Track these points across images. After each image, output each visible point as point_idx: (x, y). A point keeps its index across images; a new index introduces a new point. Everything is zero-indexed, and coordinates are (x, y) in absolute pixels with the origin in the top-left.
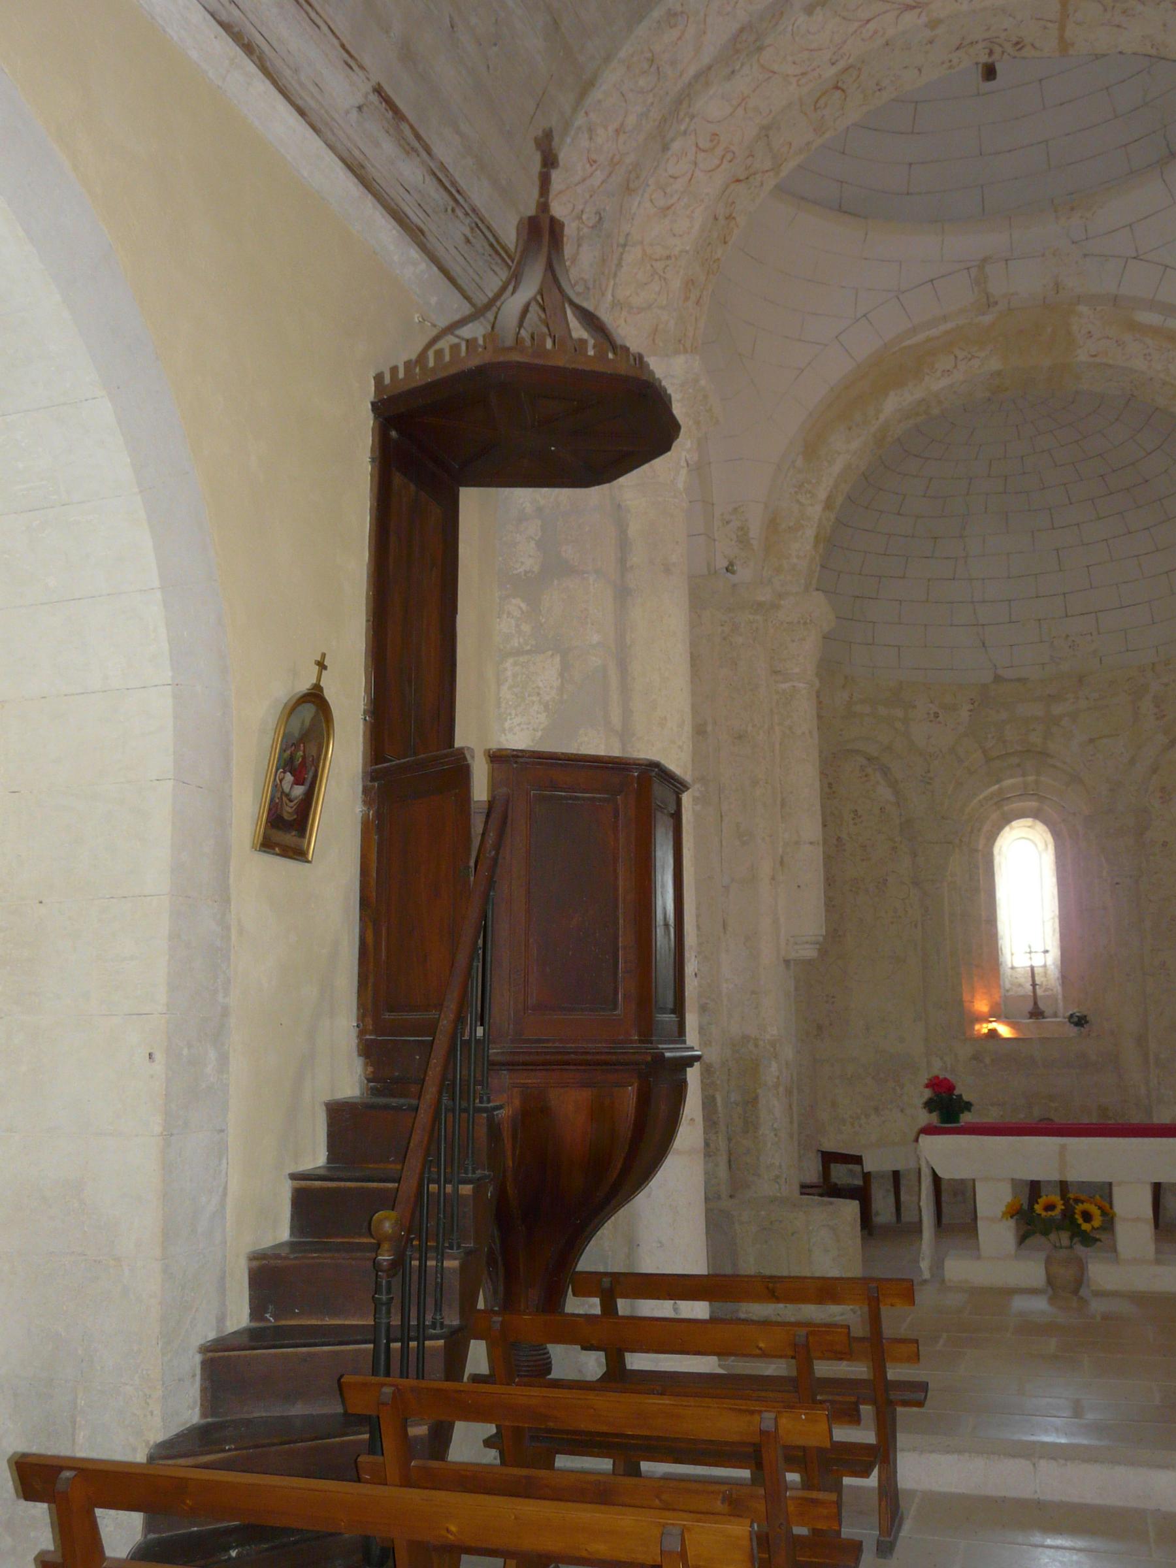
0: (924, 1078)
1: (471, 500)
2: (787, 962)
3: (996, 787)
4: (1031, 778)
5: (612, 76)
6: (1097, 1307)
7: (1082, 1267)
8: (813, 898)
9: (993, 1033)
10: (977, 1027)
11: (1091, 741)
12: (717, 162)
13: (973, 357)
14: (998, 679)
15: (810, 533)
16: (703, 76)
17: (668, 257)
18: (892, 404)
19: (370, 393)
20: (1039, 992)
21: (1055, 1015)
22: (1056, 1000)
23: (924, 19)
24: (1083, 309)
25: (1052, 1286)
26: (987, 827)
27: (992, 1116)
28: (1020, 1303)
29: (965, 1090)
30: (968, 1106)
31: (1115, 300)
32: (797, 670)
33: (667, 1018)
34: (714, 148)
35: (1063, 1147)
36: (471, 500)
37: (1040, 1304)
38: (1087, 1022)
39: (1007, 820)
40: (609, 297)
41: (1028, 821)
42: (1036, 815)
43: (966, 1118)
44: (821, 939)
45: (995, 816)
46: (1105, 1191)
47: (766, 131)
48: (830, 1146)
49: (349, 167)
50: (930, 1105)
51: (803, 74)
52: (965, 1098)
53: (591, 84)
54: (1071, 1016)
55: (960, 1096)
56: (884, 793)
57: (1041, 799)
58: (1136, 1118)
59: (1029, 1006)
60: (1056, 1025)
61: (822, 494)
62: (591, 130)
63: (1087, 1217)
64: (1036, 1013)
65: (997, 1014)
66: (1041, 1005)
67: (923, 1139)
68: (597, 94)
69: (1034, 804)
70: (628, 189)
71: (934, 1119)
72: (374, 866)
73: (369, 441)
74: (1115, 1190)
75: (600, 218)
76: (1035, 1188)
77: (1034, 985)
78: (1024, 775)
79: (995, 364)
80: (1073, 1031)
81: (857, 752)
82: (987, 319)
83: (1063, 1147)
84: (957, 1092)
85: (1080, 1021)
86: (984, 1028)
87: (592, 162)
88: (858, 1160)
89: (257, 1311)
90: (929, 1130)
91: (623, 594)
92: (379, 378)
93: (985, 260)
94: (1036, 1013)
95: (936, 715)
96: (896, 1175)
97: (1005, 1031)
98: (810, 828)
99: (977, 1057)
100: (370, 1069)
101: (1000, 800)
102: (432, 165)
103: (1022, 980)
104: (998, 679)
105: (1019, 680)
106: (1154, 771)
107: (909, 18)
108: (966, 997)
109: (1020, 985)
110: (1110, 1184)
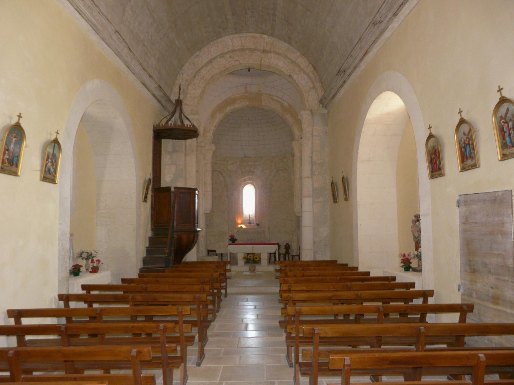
0: (458, 195)
1: (163, 141)
2: (204, 213)
3: (244, 178)
4: (251, 177)
5: (187, 65)
6: (257, 273)
7: (255, 267)
8: (210, 202)
9: (241, 227)
10: (238, 226)
11: (262, 170)
12: (204, 81)
13: (244, 101)
14: (245, 157)
15: (212, 132)
16: (202, 67)
17: (195, 97)
18: (229, 109)
19: (152, 128)
20: (251, 219)
21: (253, 223)
22: (254, 220)
23: (239, 63)
24: (264, 95)
25: (250, 270)
26: (242, 186)
27: (241, 242)
28: (245, 273)
29: (236, 237)
30: (237, 240)
31: (270, 94)
32: (208, 158)
33: (196, 225)
34: (203, 79)
35: (253, 247)
36: (163, 141)
37: (248, 273)
38: (259, 225)
39: (246, 184)
40: (184, 103)
41: (250, 185)
42: (252, 184)
43: (236, 242)
44: (211, 209)
45: (243, 184)
46: (260, 254)
47: (212, 77)
48: (209, 249)
49: (152, 95)
50: (230, 240)
51: (219, 69)
52: (236, 239)
53: (183, 66)
54: (256, 224)
55: (235, 238)
56: (222, 178)
57: (253, 181)
58: (267, 242)
59: (248, 222)
60: (254, 225)
61: (214, 125)
62: (183, 74)
63: (256, 258)
64: (250, 223)
65: (242, 223)
66: (251, 222)
67: (229, 246)
68: (184, 68)
69: (251, 182)
70: (189, 85)
71: (231, 242)
72: (153, 201)
73: (152, 136)
74: (261, 254)
75: (184, 90)
76: (248, 254)
77: (250, 217)
78: (249, 176)
79: (247, 103)
80: (256, 227)
81: (217, 170)
82: (247, 94)
83: (253, 247)
84: (235, 238)
85: (258, 225)
86: (240, 226)
87: (183, 80)
88: (215, 251)
89: (144, 265)
90: (230, 244)
91: (186, 155)
92: (154, 126)
93: (247, 84)
94: (250, 223)
95: (233, 164)
96: (222, 254)
97: (244, 226)
98: (210, 188)
99: (238, 232)
100: (153, 232)
101: (245, 180)
102: (164, 92)
103: (247, 216)
104: (245, 157)
105: (249, 157)
106: (274, 177)
107: (236, 63)
108: (236, 220)
109: (247, 217)
110: (260, 253)
